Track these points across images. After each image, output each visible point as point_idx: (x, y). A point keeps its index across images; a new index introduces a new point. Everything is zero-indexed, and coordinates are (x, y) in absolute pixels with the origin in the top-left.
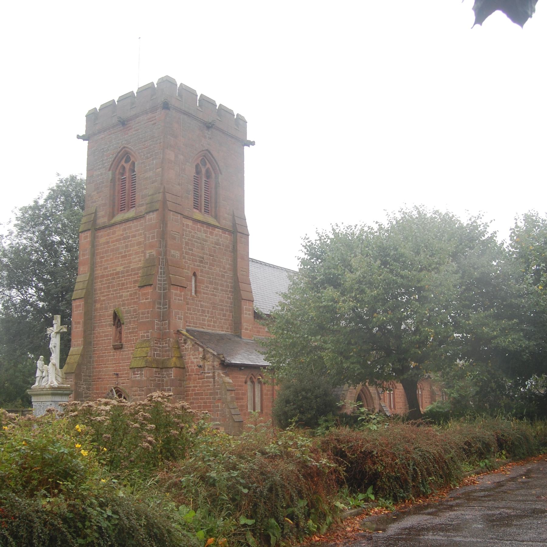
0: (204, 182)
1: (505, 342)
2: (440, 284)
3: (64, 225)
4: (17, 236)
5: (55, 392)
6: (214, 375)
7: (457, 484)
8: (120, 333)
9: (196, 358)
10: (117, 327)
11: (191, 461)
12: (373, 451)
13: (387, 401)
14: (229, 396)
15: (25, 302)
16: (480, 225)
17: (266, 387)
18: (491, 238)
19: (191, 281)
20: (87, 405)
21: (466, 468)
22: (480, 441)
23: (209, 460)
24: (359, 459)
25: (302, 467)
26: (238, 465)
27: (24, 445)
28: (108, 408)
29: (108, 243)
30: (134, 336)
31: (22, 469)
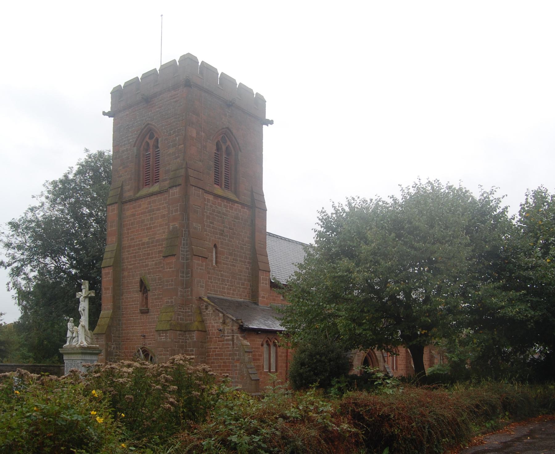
0: (224, 159)
1: (511, 312)
2: (453, 257)
3: (93, 198)
4: (49, 209)
5: (84, 351)
6: (233, 338)
7: (467, 444)
8: (147, 299)
9: (217, 323)
10: (144, 294)
11: (211, 425)
12: (390, 415)
13: (390, 363)
14: (247, 357)
15: (58, 269)
16: (492, 200)
17: (280, 350)
18: (503, 213)
19: (212, 253)
20: (109, 366)
21: (475, 429)
22: (487, 404)
23: (230, 424)
24: (376, 422)
25: (323, 432)
26: (259, 429)
27: (35, 411)
28: (130, 370)
29: (134, 215)
30: (160, 302)
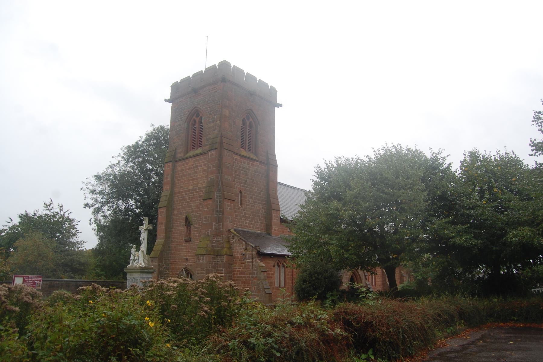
2: (414, 199)
5: (143, 270)
7: (433, 347)
8: (190, 231)
11: (236, 329)
12: (372, 322)
13: (370, 280)
14: (263, 275)
15: (127, 209)
17: (288, 270)
18: (448, 167)
22: (446, 313)
27: (103, 317)
29: (183, 170)
31: (100, 336)
